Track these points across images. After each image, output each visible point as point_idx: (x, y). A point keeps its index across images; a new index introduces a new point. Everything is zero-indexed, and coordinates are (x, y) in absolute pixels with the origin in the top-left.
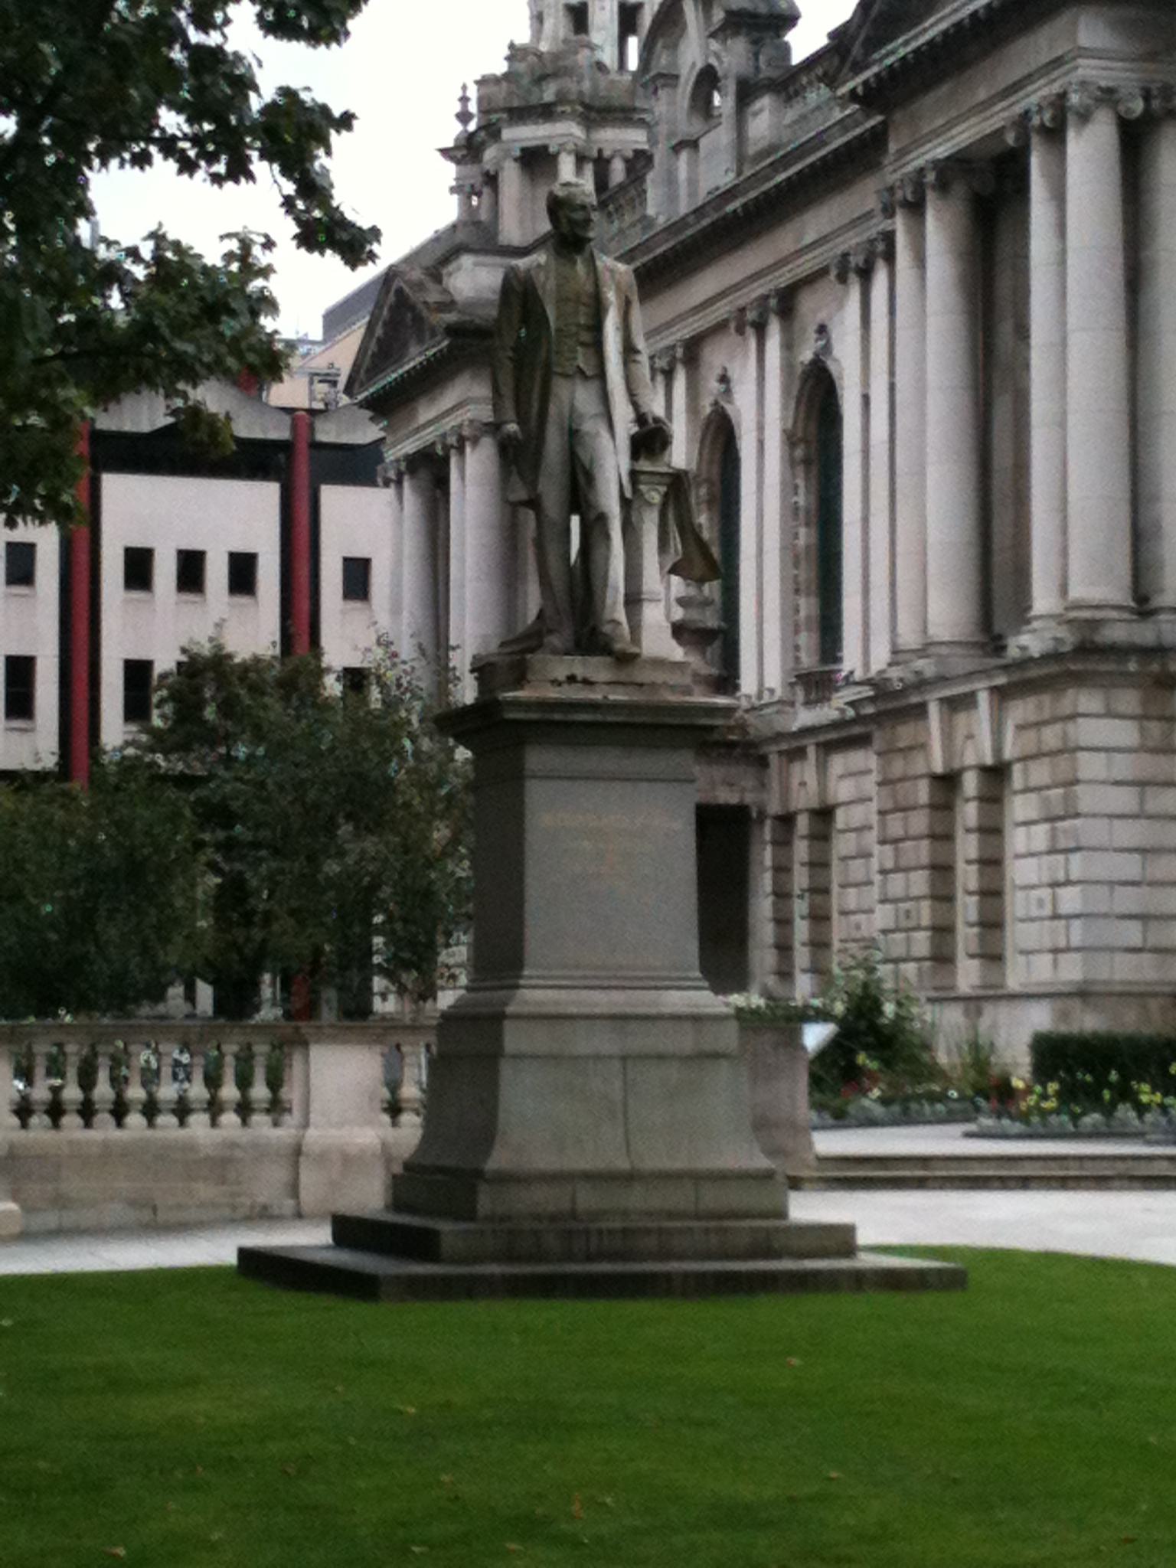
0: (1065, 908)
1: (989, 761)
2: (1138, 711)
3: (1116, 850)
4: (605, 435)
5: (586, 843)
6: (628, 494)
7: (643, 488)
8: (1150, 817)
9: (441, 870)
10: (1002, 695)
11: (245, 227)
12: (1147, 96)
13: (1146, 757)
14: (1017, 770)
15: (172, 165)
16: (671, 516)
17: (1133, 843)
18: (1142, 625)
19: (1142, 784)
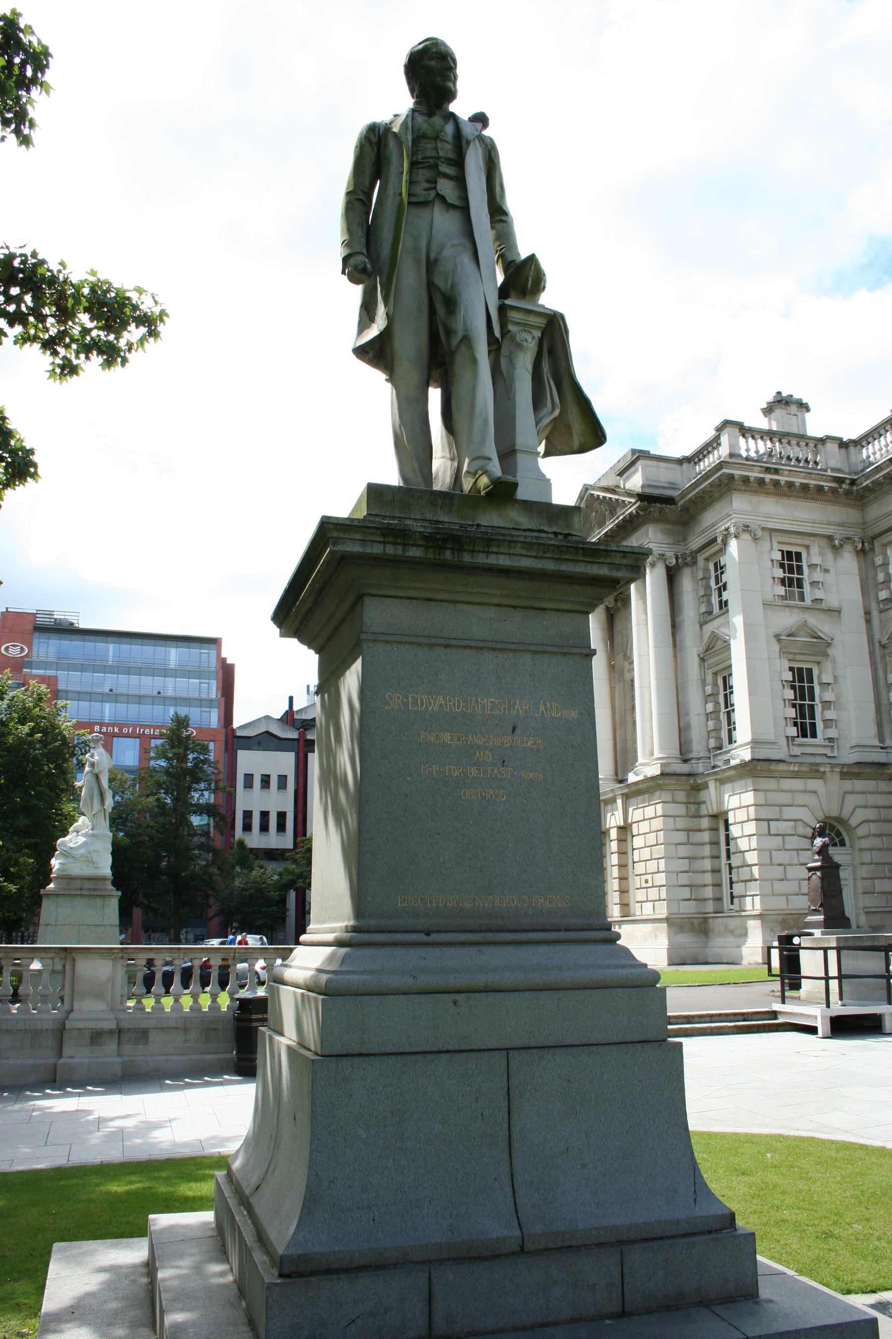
0: (657, 883)
1: (622, 824)
2: (685, 800)
3: (679, 858)
4: (466, 259)
5: (447, 737)
6: (497, 333)
7: (511, 327)
8: (691, 844)
9: (178, 730)
10: (626, 797)
11: (93, 273)
12: (677, 558)
13: (688, 819)
14: (635, 826)
15: (96, 360)
16: (546, 367)
17: (685, 855)
18: (685, 765)
19: (688, 831)
